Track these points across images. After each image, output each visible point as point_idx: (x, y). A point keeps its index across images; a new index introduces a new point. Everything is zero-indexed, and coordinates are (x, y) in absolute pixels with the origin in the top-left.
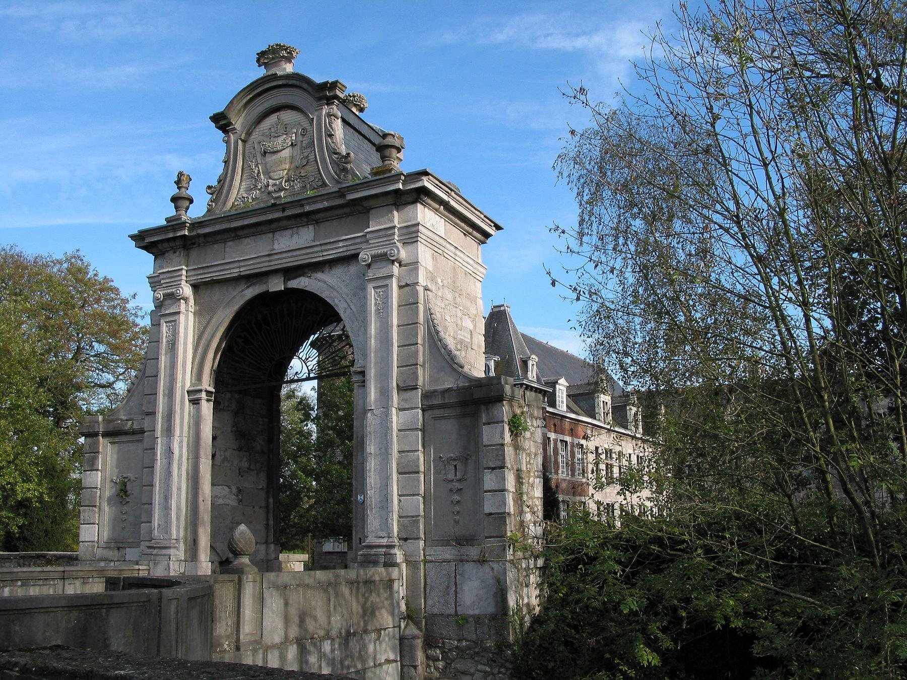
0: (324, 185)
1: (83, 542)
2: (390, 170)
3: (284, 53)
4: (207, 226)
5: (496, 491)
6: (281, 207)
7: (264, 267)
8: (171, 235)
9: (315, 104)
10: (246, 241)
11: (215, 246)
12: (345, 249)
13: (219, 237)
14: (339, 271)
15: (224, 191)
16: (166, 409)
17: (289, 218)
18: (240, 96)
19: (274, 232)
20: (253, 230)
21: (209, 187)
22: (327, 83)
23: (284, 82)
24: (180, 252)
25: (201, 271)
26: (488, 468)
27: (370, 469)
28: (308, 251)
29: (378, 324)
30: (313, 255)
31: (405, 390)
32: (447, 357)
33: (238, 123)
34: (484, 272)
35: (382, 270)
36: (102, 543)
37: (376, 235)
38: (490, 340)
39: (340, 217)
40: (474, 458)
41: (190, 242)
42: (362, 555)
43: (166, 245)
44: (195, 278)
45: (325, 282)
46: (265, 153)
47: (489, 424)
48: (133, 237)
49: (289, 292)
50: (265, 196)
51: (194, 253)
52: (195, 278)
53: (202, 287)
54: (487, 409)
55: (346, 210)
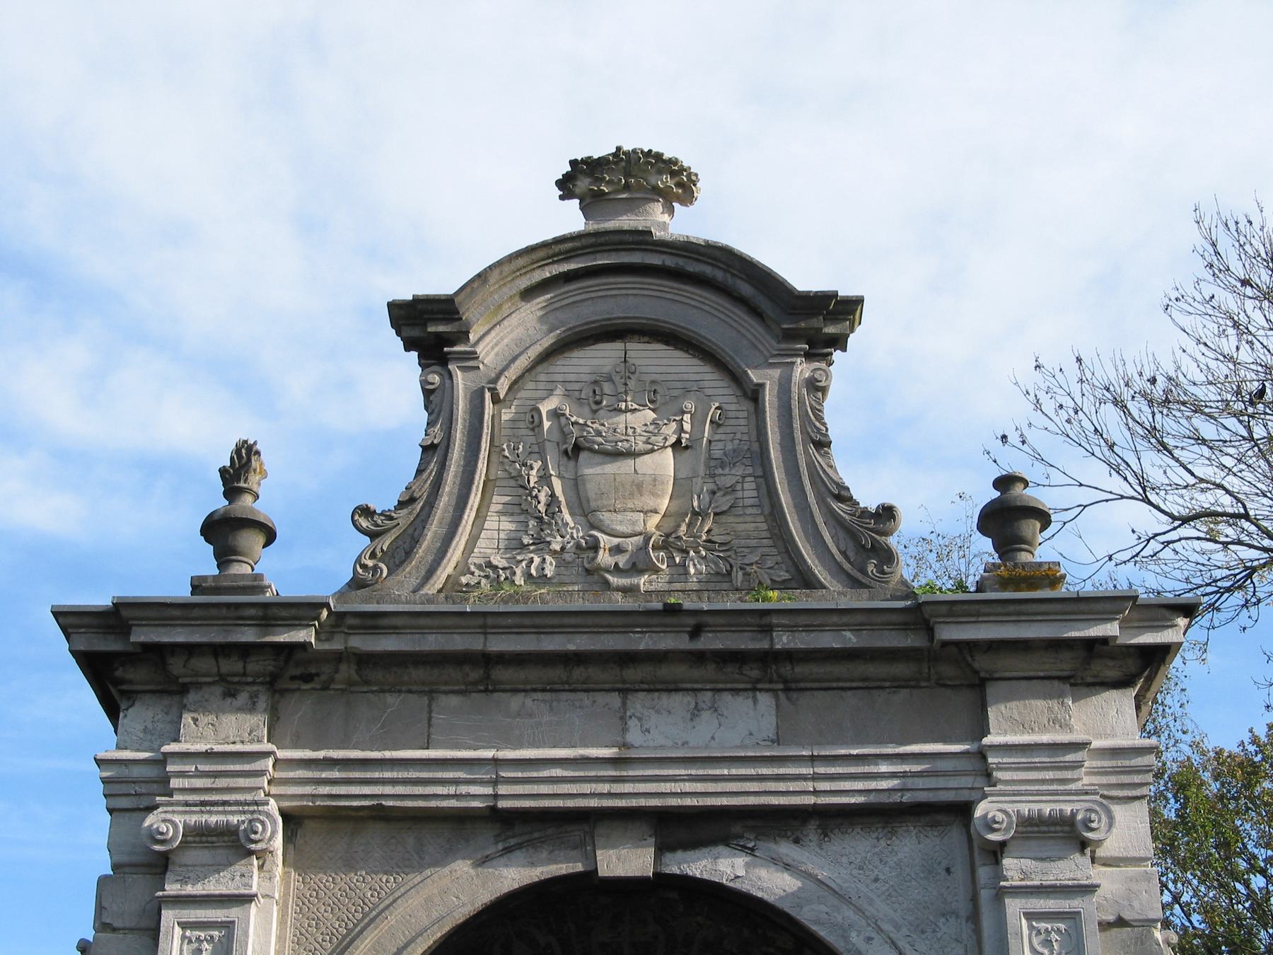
0: (806, 581)
3: (666, 181)
4: (395, 630)
6: (692, 621)
8: (248, 635)
9: (771, 344)
10: (516, 702)
11: (391, 699)
13: (418, 674)
15: (429, 535)
17: (699, 657)
18: (513, 266)
19: (625, 691)
20: (557, 673)
21: (365, 511)
23: (670, 261)
25: (336, 774)
30: (782, 786)
39: (869, 685)
41: (297, 672)
43: (204, 664)
44: (308, 790)
45: (808, 876)
46: (577, 448)
48: (69, 620)
49: (662, 881)
51: (300, 708)
52: (308, 790)
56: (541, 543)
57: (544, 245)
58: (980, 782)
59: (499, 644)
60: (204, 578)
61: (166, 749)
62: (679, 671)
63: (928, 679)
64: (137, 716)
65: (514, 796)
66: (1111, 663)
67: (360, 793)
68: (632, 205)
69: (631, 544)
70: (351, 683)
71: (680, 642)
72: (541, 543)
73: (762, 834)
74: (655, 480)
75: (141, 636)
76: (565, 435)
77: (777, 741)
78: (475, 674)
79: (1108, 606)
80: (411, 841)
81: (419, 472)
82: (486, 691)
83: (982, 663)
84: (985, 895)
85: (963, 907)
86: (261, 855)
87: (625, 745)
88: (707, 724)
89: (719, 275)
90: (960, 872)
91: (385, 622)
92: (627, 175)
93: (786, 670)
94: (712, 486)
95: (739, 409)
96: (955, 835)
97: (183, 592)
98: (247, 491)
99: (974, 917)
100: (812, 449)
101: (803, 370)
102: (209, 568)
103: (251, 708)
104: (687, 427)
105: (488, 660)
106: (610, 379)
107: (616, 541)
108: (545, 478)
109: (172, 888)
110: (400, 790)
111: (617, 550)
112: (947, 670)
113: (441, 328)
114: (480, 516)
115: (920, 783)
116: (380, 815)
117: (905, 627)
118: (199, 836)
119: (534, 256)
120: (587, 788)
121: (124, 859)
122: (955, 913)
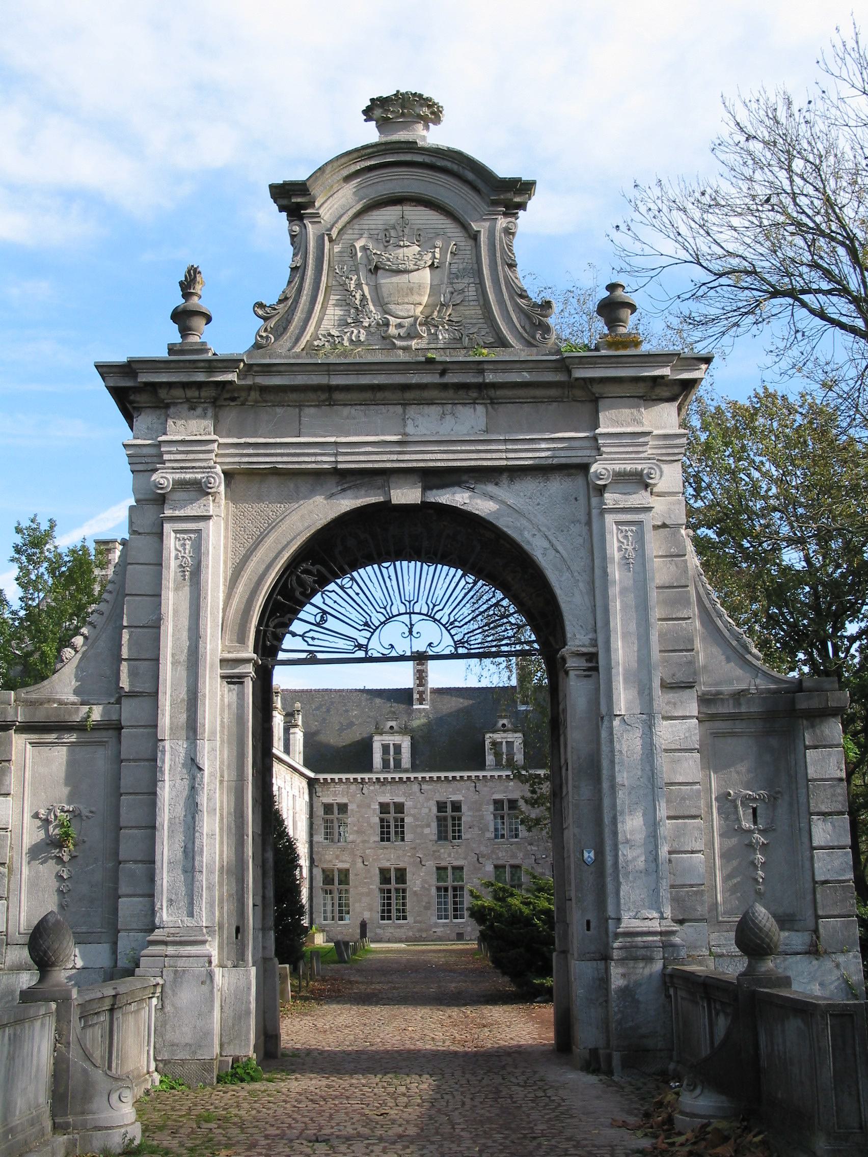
0: (502, 343)
2: (637, 344)
3: (425, 111)
6: (441, 367)
7: (386, 460)
8: (201, 377)
9: (484, 208)
10: (346, 411)
11: (279, 410)
13: (293, 396)
14: (529, 486)
17: (445, 387)
18: (339, 163)
20: (368, 395)
21: (260, 305)
22: (519, 180)
23: (427, 159)
24: (205, 409)
26: (818, 814)
30: (489, 456)
31: (672, 688)
32: (734, 643)
34: (166, 457)
39: (536, 401)
41: (228, 396)
42: (620, 948)
43: (178, 392)
44: (237, 459)
45: (502, 502)
46: (377, 268)
48: (104, 370)
49: (425, 506)
52: (237, 459)
53: (237, 477)
55: (553, 392)
56: (357, 322)
57: (356, 150)
58: (594, 453)
59: (337, 380)
61: (160, 439)
62: (434, 393)
63: (568, 397)
64: (143, 420)
65: (347, 462)
66: (665, 389)
67: (264, 461)
68: (406, 125)
69: (407, 322)
70: (256, 402)
72: (357, 322)
73: (478, 481)
74: (420, 286)
75: (143, 378)
76: (370, 261)
77: (487, 431)
78: (324, 396)
79: (665, 359)
81: (290, 282)
82: (330, 405)
83: (597, 389)
84: (595, 512)
85: (583, 518)
86: (214, 495)
87: (405, 434)
89: (455, 167)
90: (582, 500)
91: (274, 369)
92: (403, 107)
93: (492, 393)
94: (451, 289)
96: (580, 481)
97: (162, 353)
99: (589, 523)
102: (177, 338)
103: (204, 416)
104: (437, 256)
105: (330, 389)
106: (394, 228)
107: (399, 321)
108: (359, 285)
109: (168, 513)
110: (285, 459)
111: (399, 326)
112: (578, 393)
113: (299, 200)
114: (324, 307)
115: (562, 453)
117: (556, 370)
118: (181, 485)
119: (351, 157)
121: (141, 497)
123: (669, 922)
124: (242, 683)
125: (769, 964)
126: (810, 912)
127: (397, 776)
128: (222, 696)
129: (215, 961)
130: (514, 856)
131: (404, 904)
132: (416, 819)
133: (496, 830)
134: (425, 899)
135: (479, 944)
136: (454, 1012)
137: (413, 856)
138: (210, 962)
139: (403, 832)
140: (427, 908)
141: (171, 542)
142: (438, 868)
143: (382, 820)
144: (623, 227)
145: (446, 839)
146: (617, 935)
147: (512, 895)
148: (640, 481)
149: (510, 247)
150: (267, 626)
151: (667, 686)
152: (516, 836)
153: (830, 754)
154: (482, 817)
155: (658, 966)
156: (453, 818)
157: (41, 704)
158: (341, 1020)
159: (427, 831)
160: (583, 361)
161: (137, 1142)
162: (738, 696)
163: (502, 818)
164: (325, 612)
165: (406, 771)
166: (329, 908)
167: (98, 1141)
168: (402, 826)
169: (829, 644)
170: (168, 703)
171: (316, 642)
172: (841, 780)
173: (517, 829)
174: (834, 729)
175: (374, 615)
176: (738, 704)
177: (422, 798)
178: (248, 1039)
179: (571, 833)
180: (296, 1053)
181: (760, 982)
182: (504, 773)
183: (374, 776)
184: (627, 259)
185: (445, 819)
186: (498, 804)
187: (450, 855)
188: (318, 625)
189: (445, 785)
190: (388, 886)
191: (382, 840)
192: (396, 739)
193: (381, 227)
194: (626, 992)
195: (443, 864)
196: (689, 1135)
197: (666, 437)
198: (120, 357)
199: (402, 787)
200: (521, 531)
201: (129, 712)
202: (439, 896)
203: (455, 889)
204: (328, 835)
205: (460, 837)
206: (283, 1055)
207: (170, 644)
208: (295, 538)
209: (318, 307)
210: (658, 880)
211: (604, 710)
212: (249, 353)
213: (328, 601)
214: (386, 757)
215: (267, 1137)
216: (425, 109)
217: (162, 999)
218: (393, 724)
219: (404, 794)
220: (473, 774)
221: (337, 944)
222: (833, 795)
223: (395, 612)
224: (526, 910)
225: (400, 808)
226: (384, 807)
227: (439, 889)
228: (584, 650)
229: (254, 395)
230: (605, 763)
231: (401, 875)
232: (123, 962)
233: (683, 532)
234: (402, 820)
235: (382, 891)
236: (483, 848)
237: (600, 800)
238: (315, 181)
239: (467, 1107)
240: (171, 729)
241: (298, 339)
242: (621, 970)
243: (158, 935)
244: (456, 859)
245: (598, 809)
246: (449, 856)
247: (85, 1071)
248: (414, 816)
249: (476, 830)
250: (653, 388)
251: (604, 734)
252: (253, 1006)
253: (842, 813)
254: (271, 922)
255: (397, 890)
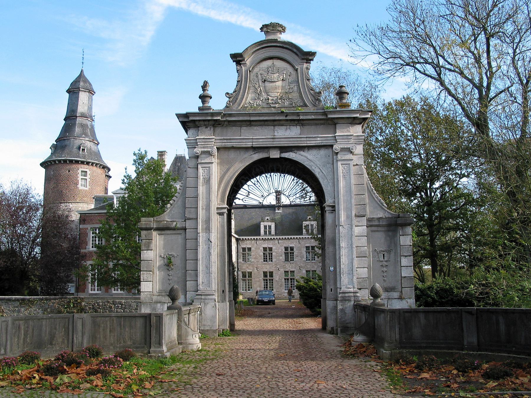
0: (306, 105)
1: (143, 292)
3: (280, 29)
5: (407, 266)
8: (209, 118)
9: (299, 61)
10: (255, 128)
11: (234, 128)
12: (321, 142)
13: (238, 123)
14: (314, 152)
16: (205, 217)
17: (287, 120)
19: (274, 126)
20: (263, 123)
21: (227, 93)
23: (281, 45)
24: (210, 128)
25: (225, 141)
26: (403, 256)
27: (342, 255)
28: (298, 139)
29: (344, 183)
30: (301, 142)
32: (378, 202)
33: (248, 61)
35: (346, 156)
36: (155, 293)
37: (341, 137)
38: (52, 185)
39: (316, 125)
40: (394, 251)
43: (202, 123)
45: (305, 157)
46: (265, 81)
47: (403, 235)
48: (179, 116)
49: (281, 158)
50: (265, 105)
54: (403, 229)
56: (259, 98)
57: (258, 42)
58: (335, 141)
59: (252, 119)
60: (200, 107)
61: (197, 138)
62: (283, 122)
64: (190, 132)
65: (255, 144)
67: (229, 144)
68: (274, 33)
69: (275, 98)
70: (227, 125)
71: (284, 118)
72: (259, 98)
75: (191, 118)
76: (263, 79)
77: (300, 134)
78: (248, 123)
79: (357, 111)
80: (238, 152)
81: (237, 86)
83: (336, 121)
84: (335, 161)
85: (331, 163)
86: (214, 156)
87: (274, 136)
88: (288, 131)
89: (290, 48)
90: (331, 156)
92: (273, 27)
93: (302, 122)
94: (289, 87)
95: (293, 73)
96: (330, 150)
97: (197, 110)
98: (207, 90)
99: (333, 164)
100: (307, 81)
101: (305, 65)
102: (201, 105)
104: (284, 76)
105: (250, 121)
106: (270, 67)
107: (272, 98)
108: (259, 86)
110: (236, 144)
111: (273, 100)
112: (330, 122)
113: (240, 59)
115: (324, 142)
116: (233, 148)
117: (323, 115)
118: (203, 152)
120: (268, 143)
121: (191, 156)
122: (330, 163)
123: (356, 289)
124: (223, 215)
125: (379, 300)
126: (400, 286)
127: (270, 238)
128: (217, 219)
129: (216, 300)
130: (313, 267)
131: (272, 285)
132: (277, 253)
133: (307, 257)
134: (280, 283)
135: (300, 299)
136: (290, 320)
137: (276, 267)
138: (215, 301)
139: (272, 258)
140: (281, 286)
141: (201, 170)
142: (285, 272)
143: (264, 254)
144: (353, 41)
145: (288, 261)
146: (340, 293)
147: (310, 281)
148: (350, 151)
149: (308, 73)
150: (231, 196)
151: (356, 216)
152: (314, 260)
153: (407, 237)
154: (301, 253)
155: (352, 303)
156: (291, 253)
157: (161, 222)
158: (252, 322)
159: (281, 258)
160: (331, 112)
161: (200, 348)
162: (379, 219)
163: (309, 253)
164: (249, 192)
165: (273, 235)
166: (244, 286)
167: (190, 347)
168: (272, 256)
169: (428, 190)
170: (201, 222)
171: (246, 202)
172: (411, 245)
173: (314, 257)
174: (409, 230)
175: (265, 193)
176: (379, 221)
177: (279, 246)
178: (227, 324)
179: (327, 261)
180: (240, 331)
181: (376, 305)
182: (310, 237)
183: (261, 238)
184: (354, 52)
185: (288, 253)
186: (307, 248)
187: (289, 267)
188: (247, 196)
189: (288, 241)
190: (266, 278)
191: (264, 261)
192: (270, 224)
193: (266, 67)
194: (342, 310)
195: (287, 270)
196: (355, 347)
197: (358, 136)
198: (184, 112)
199: (272, 241)
200: (311, 167)
201: (189, 224)
202: (285, 282)
203: (291, 279)
204: (244, 260)
205: (293, 260)
206: (236, 330)
207: (201, 203)
208: (239, 169)
209: (246, 94)
210: (353, 276)
211: (337, 224)
212: (224, 109)
213: (250, 188)
214: (265, 230)
215: (236, 349)
216: (280, 28)
217: (201, 312)
218: (268, 218)
219: (272, 244)
220: (298, 237)
221: (248, 299)
222: (408, 250)
223: (271, 192)
224: (314, 286)
225: (271, 249)
226: (265, 249)
227: (285, 279)
228: (331, 204)
229: (226, 123)
230: (337, 240)
231: (271, 274)
232: (189, 301)
233: (363, 167)
234: (272, 254)
235: (264, 280)
236: (302, 264)
237: (336, 251)
238: (245, 53)
239: (293, 342)
240: (202, 229)
241: (239, 105)
242: (341, 304)
243: (199, 292)
244: (292, 268)
245: (335, 254)
246: (289, 267)
247: (186, 329)
248: (276, 252)
249: (299, 258)
250: (354, 120)
251: (337, 231)
252: (228, 314)
253: (411, 256)
254: (232, 289)
255: (270, 280)
